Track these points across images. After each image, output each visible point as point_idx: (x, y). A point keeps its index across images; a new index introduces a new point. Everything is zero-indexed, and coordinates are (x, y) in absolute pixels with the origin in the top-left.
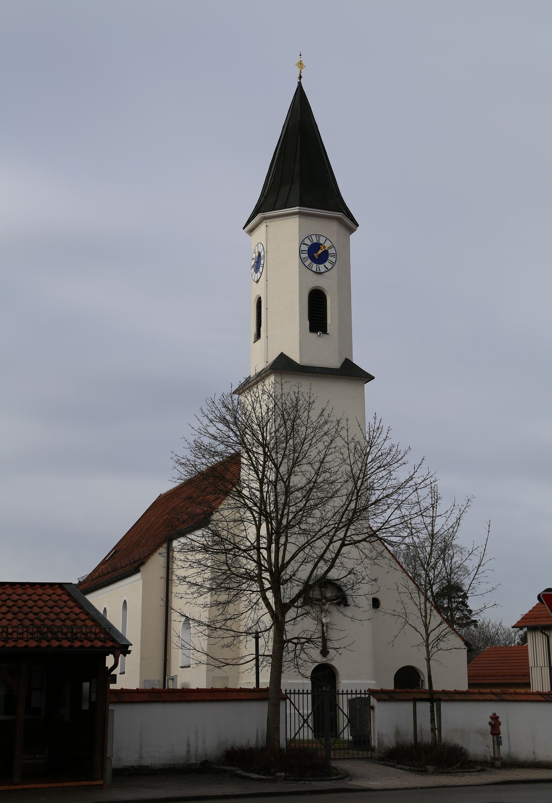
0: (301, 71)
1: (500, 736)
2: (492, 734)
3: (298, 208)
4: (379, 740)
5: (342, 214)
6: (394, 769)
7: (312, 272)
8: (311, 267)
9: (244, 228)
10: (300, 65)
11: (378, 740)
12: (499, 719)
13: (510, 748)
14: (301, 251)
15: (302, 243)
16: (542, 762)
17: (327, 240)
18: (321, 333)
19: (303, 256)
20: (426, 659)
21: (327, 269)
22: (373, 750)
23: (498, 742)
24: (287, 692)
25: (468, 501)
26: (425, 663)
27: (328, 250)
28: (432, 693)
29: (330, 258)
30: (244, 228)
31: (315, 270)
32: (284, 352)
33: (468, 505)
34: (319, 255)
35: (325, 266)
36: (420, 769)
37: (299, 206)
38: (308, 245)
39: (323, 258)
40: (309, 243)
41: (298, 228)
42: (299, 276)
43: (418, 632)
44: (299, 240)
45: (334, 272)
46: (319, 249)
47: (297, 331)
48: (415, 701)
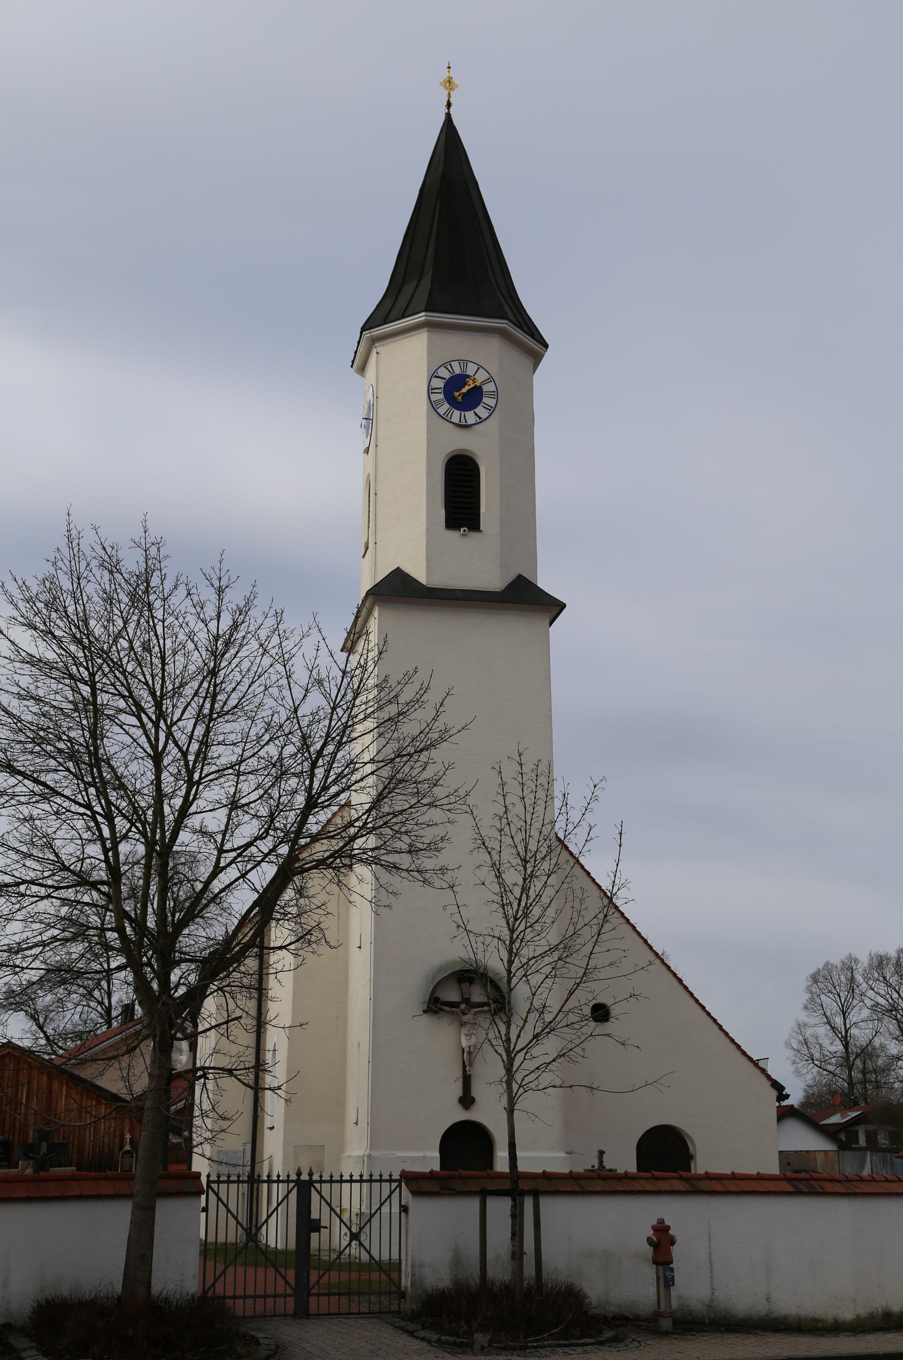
0: (449, 94)
1: (671, 1266)
2: (655, 1262)
3: (423, 314)
4: (413, 1275)
5: (506, 321)
6: (410, 1339)
7: (452, 425)
8: (449, 416)
9: (352, 366)
10: (448, 85)
11: (412, 1276)
12: (670, 1232)
13: (713, 1289)
14: (432, 389)
15: (434, 375)
16: (785, 1317)
17: (481, 369)
18: (466, 529)
19: (434, 397)
20: (505, 1109)
21: (480, 418)
22: (402, 1295)
23: (667, 1281)
24: (211, 1179)
25: (595, 787)
26: (504, 1116)
27: (483, 387)
28: (516, 1179)
29: (485, 400)
30: (352, 366)
31: (457, 421)
32: (402, 568)
33: (594, 795)
34: (465, 394)
35: (476, 414)
36: (459, 1340)
37: (426, 311)
38: (445, 379)
39: (473, 399)
40: (447, 375)
41: (426, 349)
42: (427, 432)
43: (498, 1054)
44: (428, 371)
45: (494, 422)
46: (465, 384)
47: (423, 528)
48: (484, 1194)
